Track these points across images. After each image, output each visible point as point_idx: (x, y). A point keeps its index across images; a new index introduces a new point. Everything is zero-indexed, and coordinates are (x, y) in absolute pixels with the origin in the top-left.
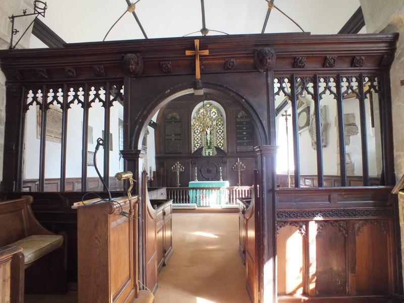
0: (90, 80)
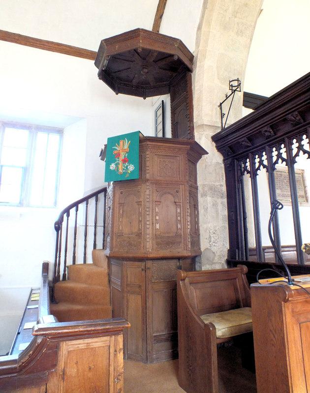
0: (289, 132)
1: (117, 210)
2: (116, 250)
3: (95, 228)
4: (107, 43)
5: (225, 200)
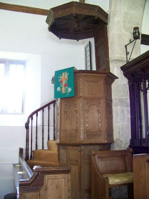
1: (63, 115)
2: (63, 140)
3: (49, 127)
4: (55, 9)
5: (129, 108)
